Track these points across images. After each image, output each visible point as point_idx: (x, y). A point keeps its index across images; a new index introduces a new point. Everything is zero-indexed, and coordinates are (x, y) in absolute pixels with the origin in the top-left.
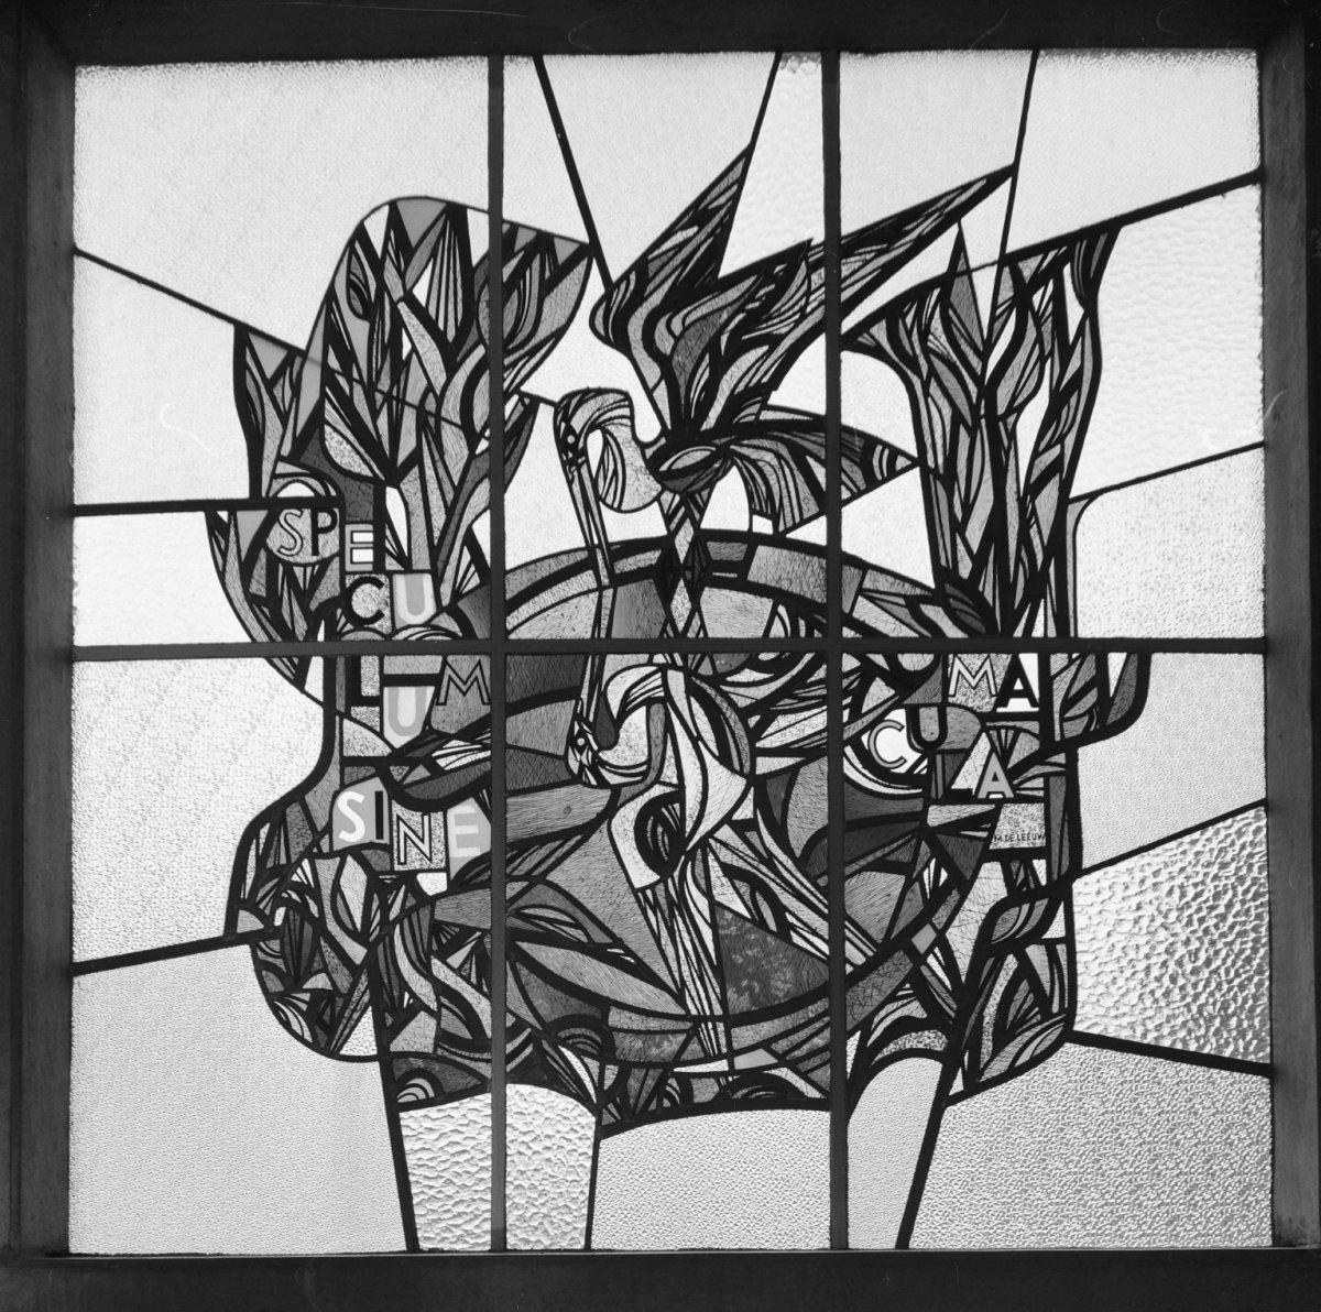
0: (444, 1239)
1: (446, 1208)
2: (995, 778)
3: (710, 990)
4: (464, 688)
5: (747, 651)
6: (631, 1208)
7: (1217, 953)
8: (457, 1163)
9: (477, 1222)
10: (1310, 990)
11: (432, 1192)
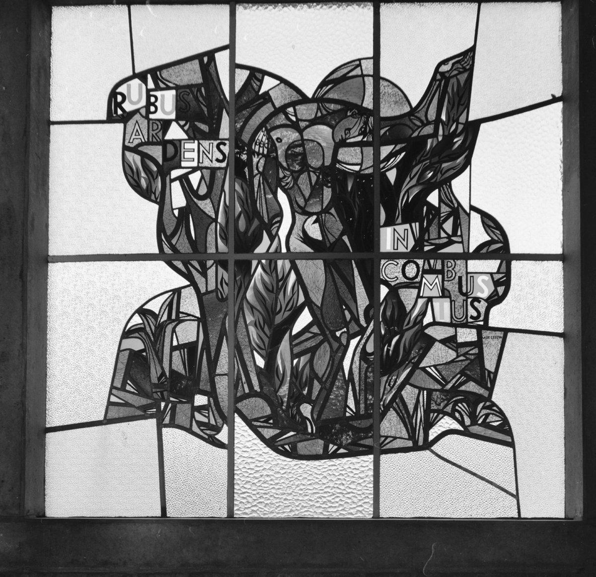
0: (318, 502)
1: (321, 488)
3: (150, 321)
4: (431, 287)
6: (415, 499)
9: (333, 497)
11: (317, 480)
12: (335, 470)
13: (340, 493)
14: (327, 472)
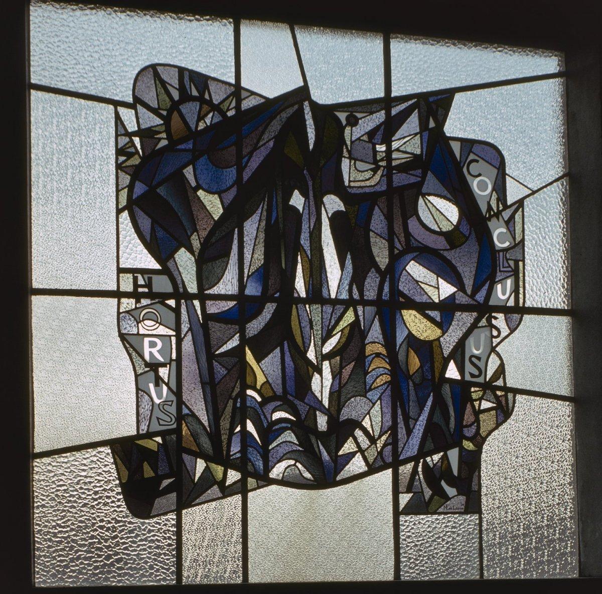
1: (50, 511)
5: (468, 439)
8: (59, 490)
10: (71, 88)
12: (64, 490)
13: (72, 516)
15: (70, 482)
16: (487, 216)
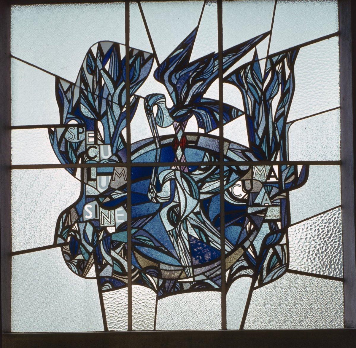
0: (115, 328)
1: (115, 319)
2: (266, 200)
4: (120, 176)
7: (328, 247)
9: (124, 323)
14: (117, 309)
15: (123, 301)
16: (83, 123)
